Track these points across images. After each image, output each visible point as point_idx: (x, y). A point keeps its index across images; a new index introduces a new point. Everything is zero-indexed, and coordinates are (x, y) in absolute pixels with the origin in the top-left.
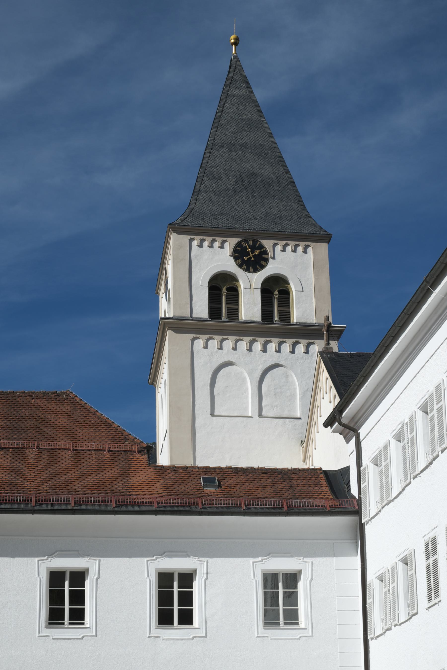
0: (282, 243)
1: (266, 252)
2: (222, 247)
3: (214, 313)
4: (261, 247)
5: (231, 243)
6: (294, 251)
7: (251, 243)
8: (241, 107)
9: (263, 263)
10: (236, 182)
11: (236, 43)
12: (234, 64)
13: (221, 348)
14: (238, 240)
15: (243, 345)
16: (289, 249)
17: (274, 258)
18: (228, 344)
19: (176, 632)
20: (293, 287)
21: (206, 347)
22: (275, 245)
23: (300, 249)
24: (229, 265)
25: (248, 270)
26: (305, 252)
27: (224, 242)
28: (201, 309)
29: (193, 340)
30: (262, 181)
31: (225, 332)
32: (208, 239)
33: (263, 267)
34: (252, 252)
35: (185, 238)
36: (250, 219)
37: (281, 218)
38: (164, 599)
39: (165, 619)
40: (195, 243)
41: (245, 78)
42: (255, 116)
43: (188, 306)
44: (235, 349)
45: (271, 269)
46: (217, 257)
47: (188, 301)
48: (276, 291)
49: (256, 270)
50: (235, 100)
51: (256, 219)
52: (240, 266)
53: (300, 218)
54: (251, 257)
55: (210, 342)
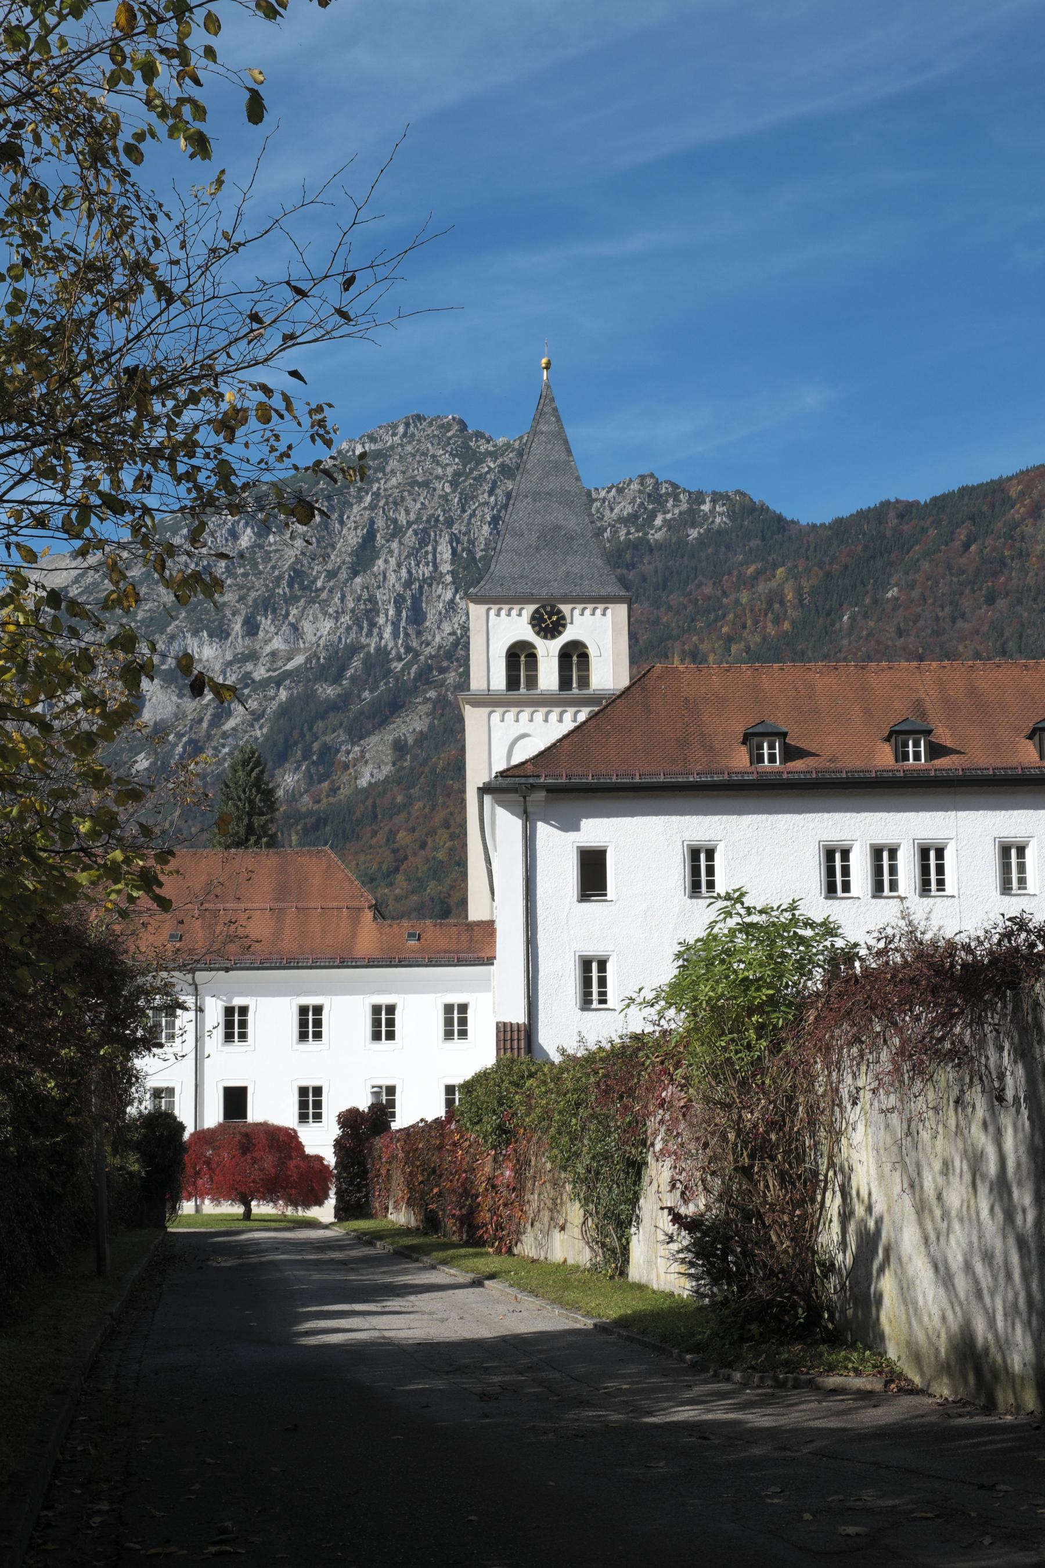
0: (580, 607)
1: (563, 618)
2: (520, 615)
3: (512, 682)
4: (559, 612)
5: (529, 610)
6: (593, 614)
7: (549, 609)
8: (549, 447)
9: (560, 628)
10: (538, 537)
11: (547, 368)
12: (544, 394)
13: (517, 721)
14: (537, 606)
15: (539, 716)
16: (587, 612)
17: (572, 623)
18: (525, 716)
19: (384, 1044)
20: (592, 652)
21: (503, 721)
22: (573, 609)
23: (598, 612)
25: (545, 637)
26: (604, 614)
27: (521, 609)
28: (499, 681)
29: (490, 713)
30: (565, 535)
31: (521, 704)
32: (506, 607)
33: (560, 633)
34: (550, 618)
35: (483, 608)
36: (550, 581)
37: (581, 577)
38: (376, 1023)
39: (376, 1036)
40: (492, 613)
41: (555, 410)
42: (563, 456)
43: (485, 678)
44: (531, 720)
45: (569, 634)
46: (514, 625)
47: (485, 674)
48: (574, 658)
49: (553, 637)
51: (556, 580)
52: (538, 634)
53: (601, 576)
54: (549, 623)
55: (507, 714)
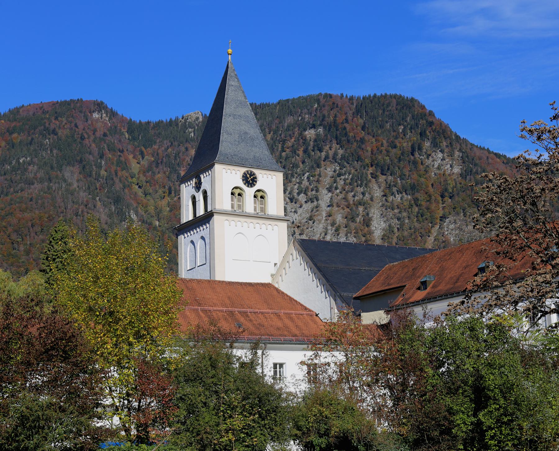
8: (236, 93)
24: (241, 184)
25: (248, 186)
33: (254, 185)
49: (252, 187)
50: (233, 88)
52: (245, 184)
54: (250, 180)
